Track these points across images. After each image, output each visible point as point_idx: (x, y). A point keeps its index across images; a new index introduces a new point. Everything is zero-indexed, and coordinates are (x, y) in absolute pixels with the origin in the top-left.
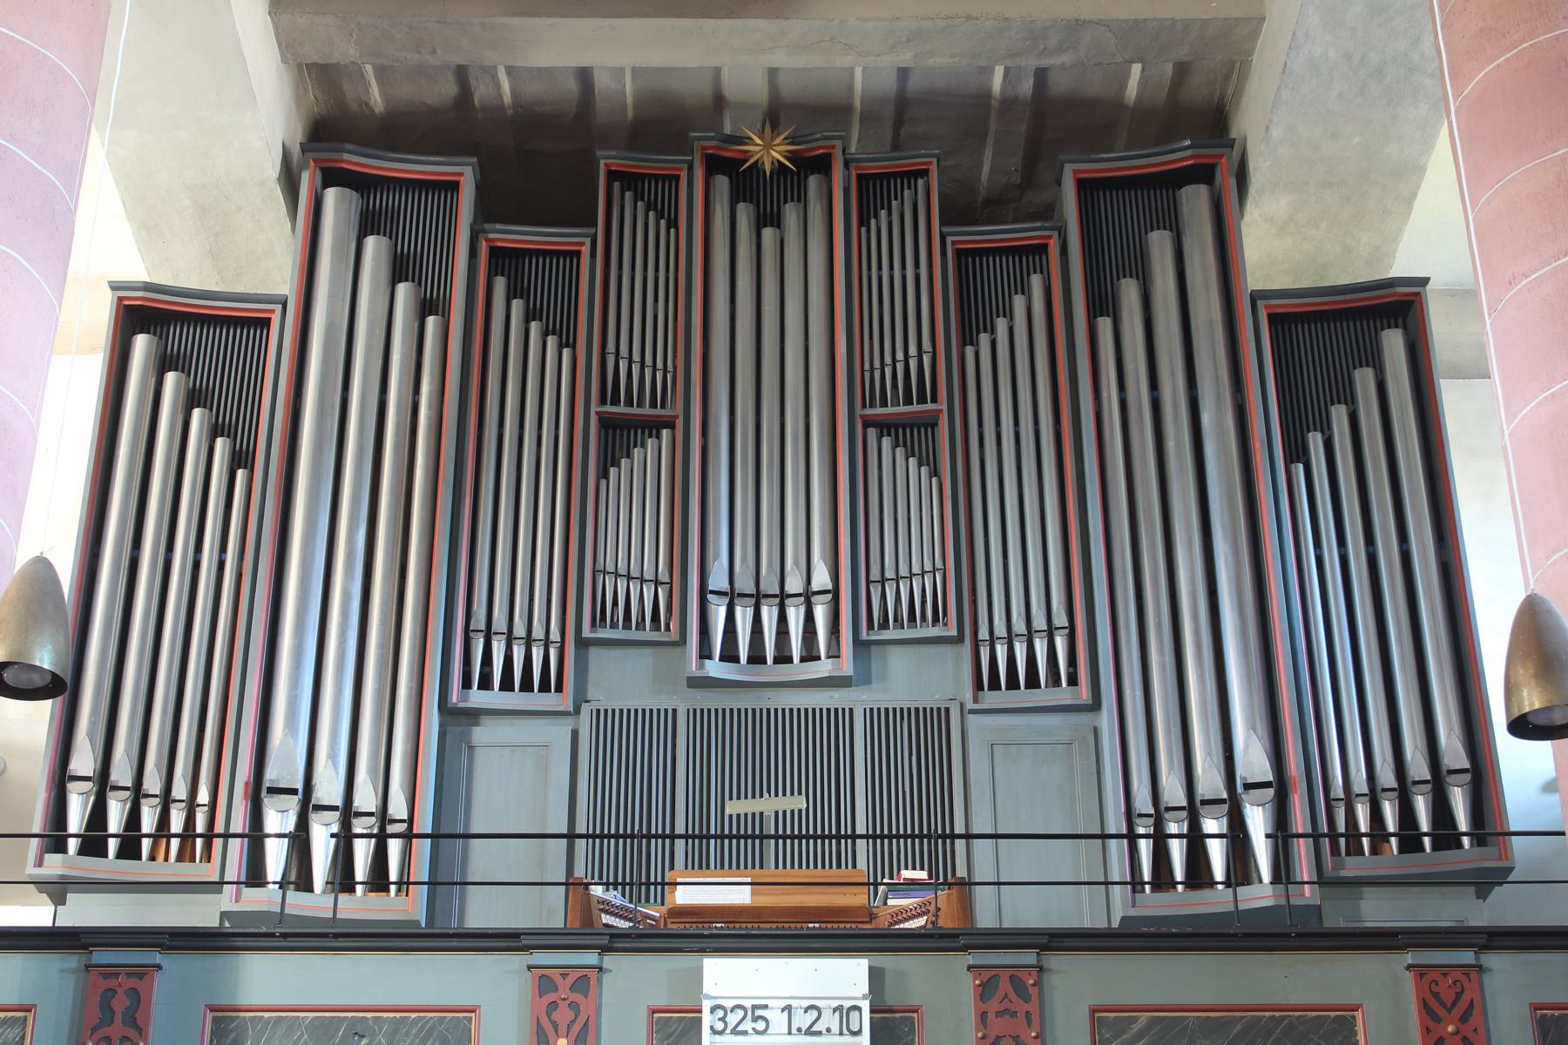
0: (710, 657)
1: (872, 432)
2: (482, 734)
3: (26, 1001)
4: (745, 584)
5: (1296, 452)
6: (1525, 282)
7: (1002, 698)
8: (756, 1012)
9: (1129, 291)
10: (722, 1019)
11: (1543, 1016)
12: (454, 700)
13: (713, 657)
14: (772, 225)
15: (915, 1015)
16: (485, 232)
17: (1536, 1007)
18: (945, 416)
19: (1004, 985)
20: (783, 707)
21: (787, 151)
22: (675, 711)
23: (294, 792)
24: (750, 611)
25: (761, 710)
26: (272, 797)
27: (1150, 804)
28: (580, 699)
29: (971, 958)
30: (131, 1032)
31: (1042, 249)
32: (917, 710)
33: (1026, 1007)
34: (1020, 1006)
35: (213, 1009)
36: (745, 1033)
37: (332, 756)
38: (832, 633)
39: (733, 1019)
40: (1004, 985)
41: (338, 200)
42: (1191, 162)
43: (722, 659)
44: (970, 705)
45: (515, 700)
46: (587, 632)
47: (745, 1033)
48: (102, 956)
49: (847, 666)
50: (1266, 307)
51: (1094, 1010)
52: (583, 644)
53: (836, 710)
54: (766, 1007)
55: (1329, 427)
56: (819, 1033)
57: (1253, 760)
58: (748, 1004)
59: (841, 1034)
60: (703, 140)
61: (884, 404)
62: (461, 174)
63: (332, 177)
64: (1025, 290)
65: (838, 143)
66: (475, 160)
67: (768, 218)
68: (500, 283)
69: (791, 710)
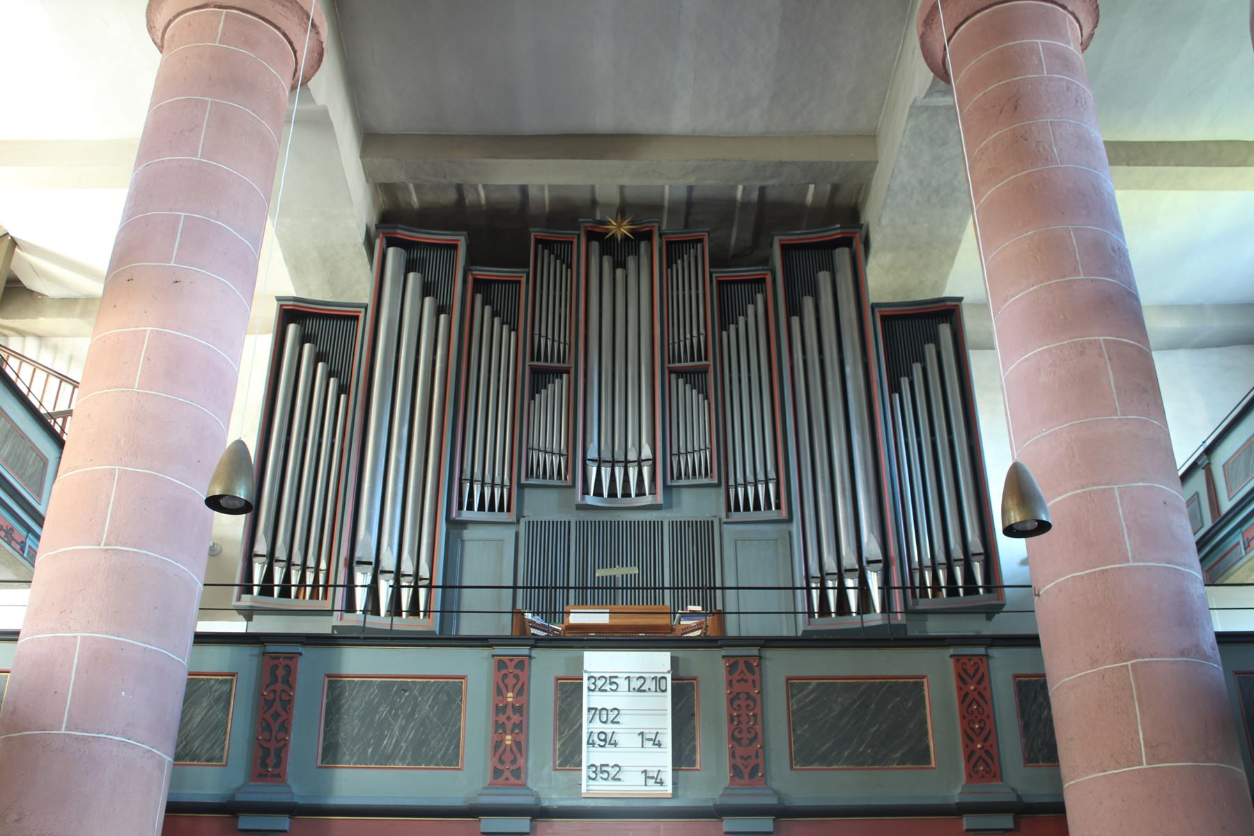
0: (588, 494)
1: (673, 376)
2: (468, 534)
3: (233, 671)
4: (606, 455)
5: (895, 387)
6: (1012, 300)
7: (741, 516)
8: (612, 680)
9: (808, 303)
10: (593, 683)
11: (1020, 681)
12: (454, 515)
14: (621, 267)
15: (695, 682)
16: (471, 270)
17: (1016, 676)
18: (712, 368)
19: (741, 666)
21: (630, 229)
22: (569, 522)
23: (370, 563)
24: (609, 470)
27: (818, 571)
28: (520, 516)
29: (724, 652)
30: (286, 688)
31: (762, 281)
32: (696, 522)
33: (752, 677)
34: (750, 677)
35: (329, 676)
36: (606, 691)
37: (390, 545)
39: (599, 683)
40: (741, 666)
41: (395, 254)
43: (595, 495)
45: (486, 516)
46: (523, 481)
47: (606, 691)
48: (271, 648)
50: (880, 312)
51: (788, 679)
52: (521, 487)
53: (654, 522)
54: (616, 677)
55: (912, 375)
56: (644, 691)
57: (872, 548)
58: (607, 675)
59: (656, 691)
60: (585, 223)
61: (680, 361)
62: (459, 240)
63: (391, 242)
64: (754, 302)
65: (656, 225)
66: (465, 233)
67: (619, 264)
68: (479, 298)
69: (631, 522)
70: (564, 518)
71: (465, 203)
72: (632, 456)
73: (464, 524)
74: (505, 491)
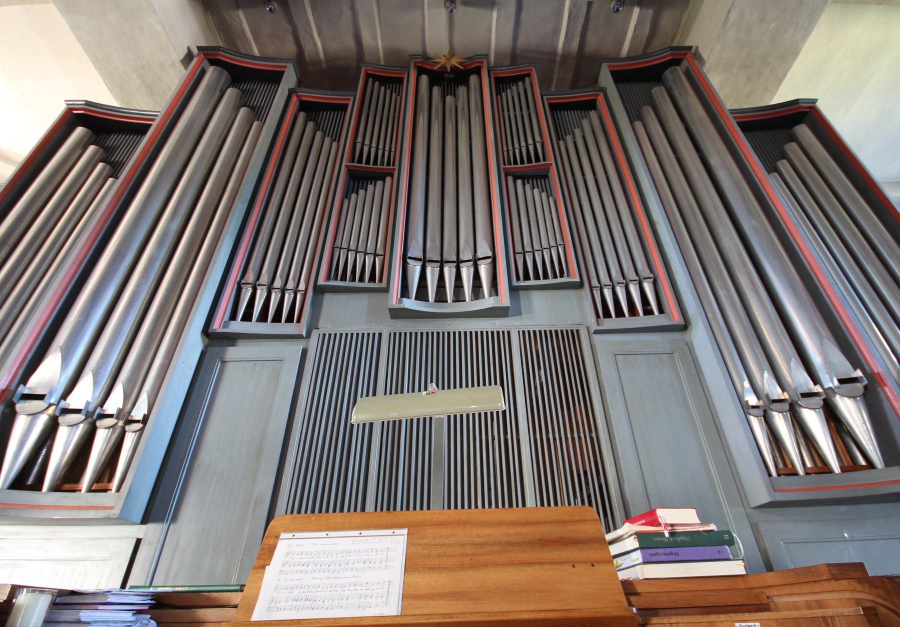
7: (613, 323)
13: (410, 296)
20: (459, 331)
22: (380, 334)
25: (443, 333)
26: (25, 403)
28: (313, 325)
38: (492, 287)
42: (670, 58)
44: (594, 327)
49: (504, 299)
52: (319, 291)
53: (498, 332)
62: (285, 67)
69: (465, 333)
70: (375, 329)
71: (305, 58)
72: (466, 255)
73: (232, 339)
74: (299, 296)
